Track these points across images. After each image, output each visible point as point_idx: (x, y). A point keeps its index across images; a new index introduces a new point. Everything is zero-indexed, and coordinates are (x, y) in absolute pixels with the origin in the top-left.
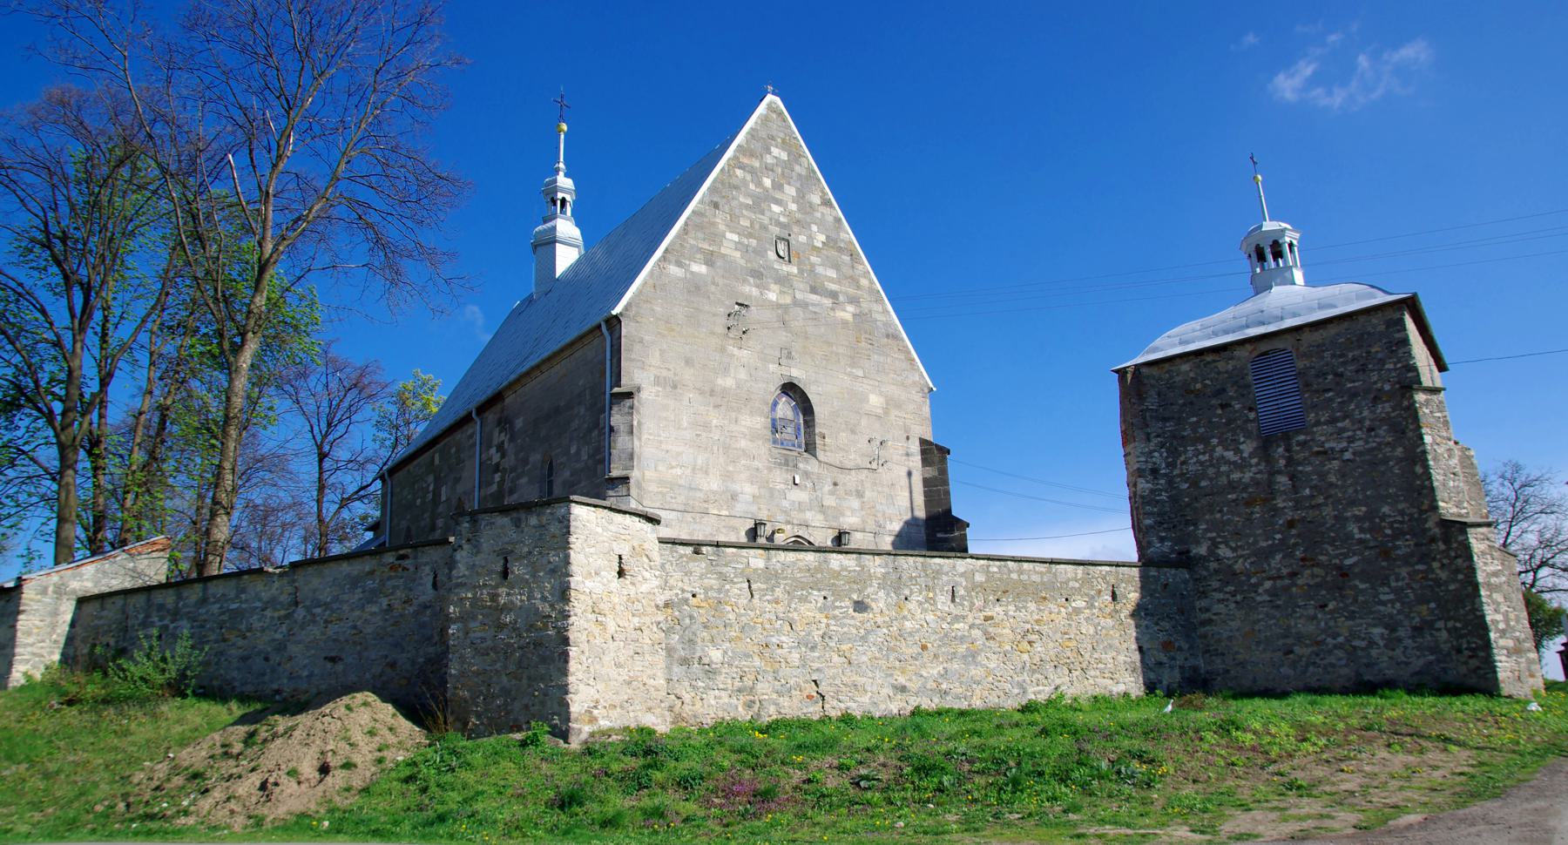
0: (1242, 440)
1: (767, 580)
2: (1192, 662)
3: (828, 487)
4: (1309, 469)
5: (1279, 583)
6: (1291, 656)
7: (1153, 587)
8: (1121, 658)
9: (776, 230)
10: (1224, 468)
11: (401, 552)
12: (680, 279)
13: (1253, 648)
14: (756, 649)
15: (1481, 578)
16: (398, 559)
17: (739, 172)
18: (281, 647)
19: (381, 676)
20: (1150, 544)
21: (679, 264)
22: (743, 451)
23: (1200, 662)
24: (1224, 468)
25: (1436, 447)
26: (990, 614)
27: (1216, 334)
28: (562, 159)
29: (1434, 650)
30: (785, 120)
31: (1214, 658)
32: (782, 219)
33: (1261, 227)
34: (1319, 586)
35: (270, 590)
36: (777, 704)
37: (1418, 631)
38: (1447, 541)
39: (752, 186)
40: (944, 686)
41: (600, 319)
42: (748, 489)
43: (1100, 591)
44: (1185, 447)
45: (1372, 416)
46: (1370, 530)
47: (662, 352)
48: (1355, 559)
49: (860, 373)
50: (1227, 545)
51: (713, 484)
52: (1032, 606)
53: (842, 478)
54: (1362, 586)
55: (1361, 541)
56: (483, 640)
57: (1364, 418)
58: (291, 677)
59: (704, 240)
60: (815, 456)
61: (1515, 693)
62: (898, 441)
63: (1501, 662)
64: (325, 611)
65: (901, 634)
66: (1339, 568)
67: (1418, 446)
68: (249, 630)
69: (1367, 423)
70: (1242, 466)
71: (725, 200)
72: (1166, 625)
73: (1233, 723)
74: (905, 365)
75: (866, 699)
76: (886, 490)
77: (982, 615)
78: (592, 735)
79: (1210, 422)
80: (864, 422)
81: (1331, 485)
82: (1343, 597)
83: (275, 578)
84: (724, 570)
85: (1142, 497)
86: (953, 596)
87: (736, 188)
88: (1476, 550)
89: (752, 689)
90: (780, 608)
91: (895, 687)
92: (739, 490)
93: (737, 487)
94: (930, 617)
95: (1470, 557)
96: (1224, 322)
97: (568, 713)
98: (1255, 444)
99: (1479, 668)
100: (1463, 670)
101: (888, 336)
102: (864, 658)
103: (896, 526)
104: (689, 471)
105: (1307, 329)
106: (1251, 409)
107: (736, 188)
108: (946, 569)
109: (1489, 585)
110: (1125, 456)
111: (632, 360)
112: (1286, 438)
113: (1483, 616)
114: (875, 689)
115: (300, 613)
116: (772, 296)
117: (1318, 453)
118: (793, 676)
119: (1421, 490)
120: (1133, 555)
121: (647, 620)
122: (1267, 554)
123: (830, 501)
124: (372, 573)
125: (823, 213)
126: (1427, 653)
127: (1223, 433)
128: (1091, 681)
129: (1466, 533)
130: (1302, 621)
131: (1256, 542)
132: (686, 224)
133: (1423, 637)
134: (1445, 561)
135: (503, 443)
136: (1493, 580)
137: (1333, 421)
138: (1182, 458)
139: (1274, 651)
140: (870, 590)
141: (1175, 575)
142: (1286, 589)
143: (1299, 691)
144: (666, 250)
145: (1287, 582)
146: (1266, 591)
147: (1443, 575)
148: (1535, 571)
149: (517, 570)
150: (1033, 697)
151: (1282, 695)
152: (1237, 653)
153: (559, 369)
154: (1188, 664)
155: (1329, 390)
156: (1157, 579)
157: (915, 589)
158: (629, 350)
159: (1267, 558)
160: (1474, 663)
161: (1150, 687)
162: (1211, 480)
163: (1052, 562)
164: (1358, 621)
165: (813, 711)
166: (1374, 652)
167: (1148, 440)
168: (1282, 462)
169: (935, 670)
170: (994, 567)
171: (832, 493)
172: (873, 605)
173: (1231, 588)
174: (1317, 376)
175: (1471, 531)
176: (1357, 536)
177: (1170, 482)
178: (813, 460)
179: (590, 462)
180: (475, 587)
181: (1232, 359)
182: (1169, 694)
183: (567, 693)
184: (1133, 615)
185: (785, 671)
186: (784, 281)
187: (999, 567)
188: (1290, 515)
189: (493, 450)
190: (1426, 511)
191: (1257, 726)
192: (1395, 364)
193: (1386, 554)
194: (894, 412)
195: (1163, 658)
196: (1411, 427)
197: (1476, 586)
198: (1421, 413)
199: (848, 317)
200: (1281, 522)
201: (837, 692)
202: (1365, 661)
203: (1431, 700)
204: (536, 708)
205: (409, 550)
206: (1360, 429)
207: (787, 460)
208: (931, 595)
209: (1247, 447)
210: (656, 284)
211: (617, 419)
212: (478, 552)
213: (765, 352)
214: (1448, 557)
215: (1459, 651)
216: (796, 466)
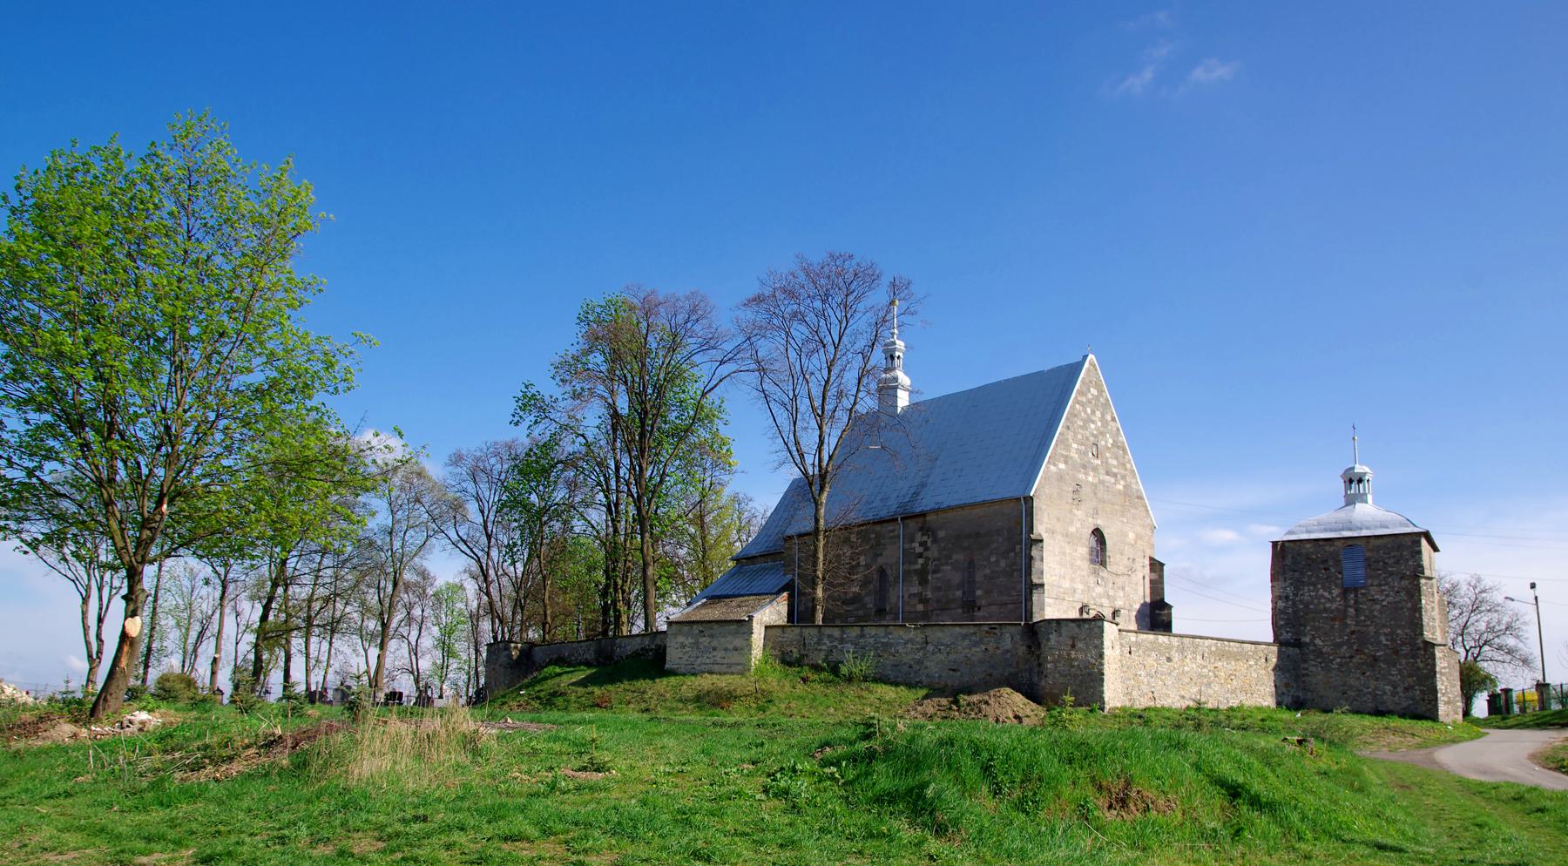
3: (1111, 585)
10: (1323, 601)
15: (1438, 669)
17: (1077, 406)
18: (919, 662)
20: (1281, 634)
21: (1054, 465)
23: (1301, 694)
27: (1326, 530)
34: (1363, 664)
37: (1407, 689)
38: (1425, 651)
42: (1080, 587)
51: (1066, 584)
52: (1233, 663)
55: (1385, 645)
65: (1183, 673)
66: (1374, 656)
70: (1331, 601)
74: (1144, 514)
81: (1375, 616)
87: (1076, 416)
93: (1075, 586)
95: (1434, 659)
103: (1137, 606)
107: (1076, 416)
109: (1441, 673)
112: (1356, 590)
115: (930, 648)
116: (1090, 479)
118: (1145, 689)
119: (1417, 624)
120: (1270, 639)
122: (1340, 645)
124: (975, 633)
137: (1380, 585)
142: (1347, 663)
147: (1421, 665)
148: (1481, 647)
149: (1080, 645)
153: (976, 511)
160: (1429, 706)
161: (1279, 704)
163: (1243, 642)
165: (1152, 704)
166: (1385, 697)
167: (1285, 581)
168: (1352, 602)
170: (1219, 643)
171: (1112, 588)
173: (1319, 660)
177: (1294, 603)
184: (1274, 670)
185: (1143, 687)
186: (1095, 469)
188: (1353, 628)
189: (916, 545)
193: (1396, 652)
194: (1139, 542)
197: (1435, 673)
203: (1408, 721)
209: (1336, 592)
210: (1045, 478)
211: (1034, 553)
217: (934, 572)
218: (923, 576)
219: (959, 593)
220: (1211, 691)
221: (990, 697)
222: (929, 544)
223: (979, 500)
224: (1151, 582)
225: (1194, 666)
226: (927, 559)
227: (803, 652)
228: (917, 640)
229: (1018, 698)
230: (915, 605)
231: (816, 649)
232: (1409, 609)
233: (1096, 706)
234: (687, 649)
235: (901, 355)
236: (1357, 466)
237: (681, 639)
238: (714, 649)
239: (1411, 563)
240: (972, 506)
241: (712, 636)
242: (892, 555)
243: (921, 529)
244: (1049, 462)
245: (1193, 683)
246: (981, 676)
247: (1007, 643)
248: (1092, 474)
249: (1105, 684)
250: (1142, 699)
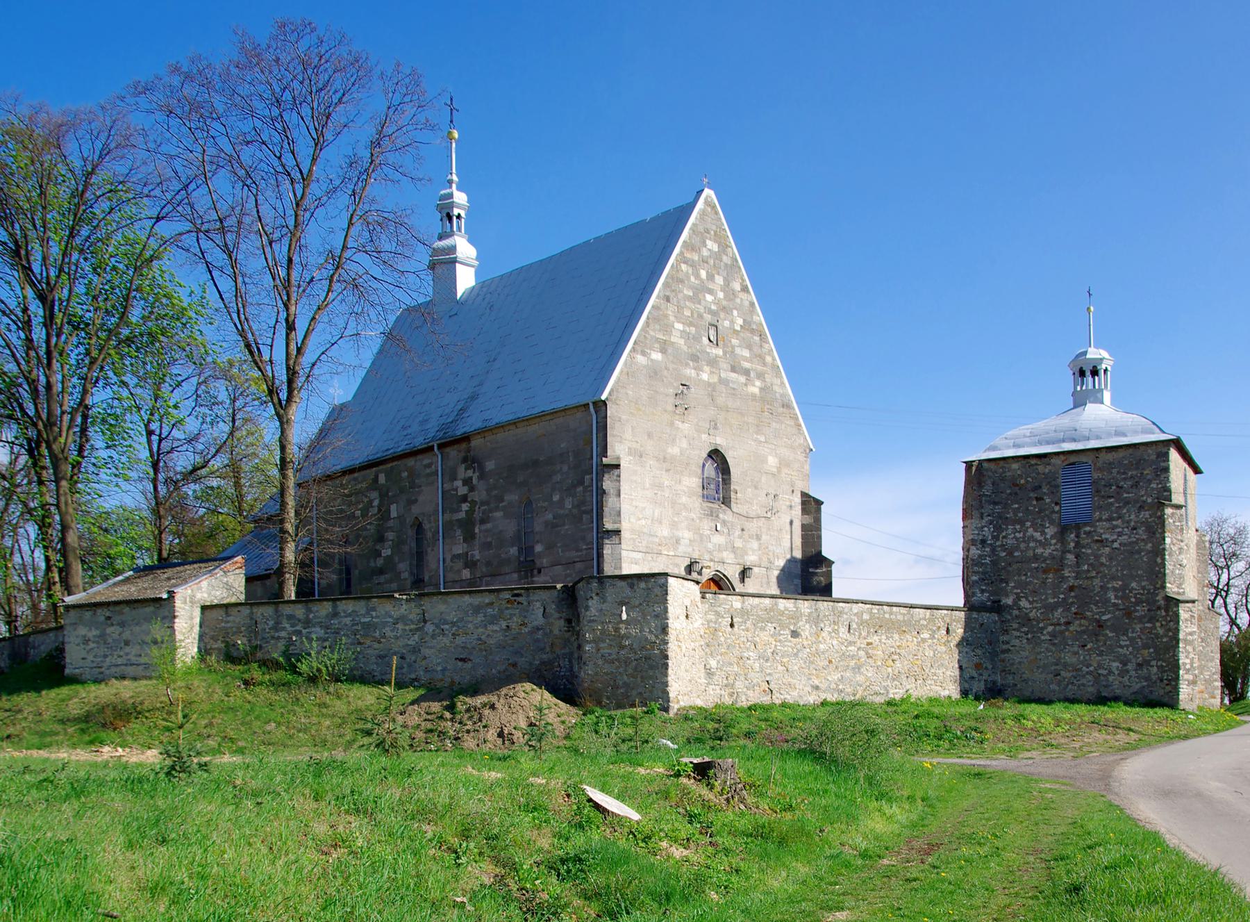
0: (1047, 525)
1: (742, 616)
2: (993, 677)
3: (738, 533)
4: (1089, 551)
5: (1058, 628)
6: (1058, 677)
7: (973, 625)
8: (948, 673)
9: (708, 317)
10: (1032, 544)
11: (515, 592)
12: (645, 367)
13: (1035, 670)
14: (735, 660)
15: (1181, 636)
16: (512, 596)
17: (684, 267)
18: (415, 650)
19: (504, 671)
20: (974, 594)
21: (644, 354)
22: (684, 505)
23: (998, 678)
24: (1032, 544)
25: (1172, 546)
26: (870, 641)
27: (1040, 443)
28: (454, 171)
29: (1147, 679)
30: (717, 213)
31: (1007, 675)
32: (713, 307)
33: (1085, 353)
34: (1084, 632)
35: (399, 609)
36: (746, 695)
37: (1140, 665)
38: (1167, 611)
39: (692, 279)
40: (840, 687)
41: (589, 399)
42: (686, 535)
43: (939, 627)
44: (1007, 525)
45: (1136, 519)
46: (1121, 598)
47: (633, 428)
48: (1109, 616)
49: (763, 439)
50: (1027, 599)
51: (664, 531)
52: (896, 636)
53: (748, 525)
54: (1110, 635)
55: (1115, 605)
56: (610, 654)
57: (1131, 520)
58: (426, 670)
59: (660, 331)
60: (730, 508)
62: (786, 494)
64: (453, 627)
65: (817, 653)
66: (1098, 621)
67: (1161, 545)
68: (384, 637)
69: (1132, 524)
71: (674, 294)
72: (979, 652)
73: (1022, 716)
75: (795, 693)
76: (776, 533)
77: (865, 641)
78: (678, 710)
79: (1027, 509)
80: (764, 479)
81: (1102, 564)
82: (1097, 640)
83: (403, 602)
84: (719, 609)
85: (973, 560)
86: (849, 629)
87: (682, 281)
89: (733, 685)
90: (749, 634)
91: (812, 686)
92: (681, 535)
93: (680, 534)
94: (835, 642)
95: (1178, 623)
96: (1047, 433)
97: (669, 698)
98: (1056, 530)
99: (1170, 692)
100: (1162, 692)
101: (783, 406)
102: (796, 668)
103: (781, 563)
104: (650, 521)
105: (1104, 450)
106: (1057, 504)
108: (846, 610)
110: (963, 527)
111: (614, 436)
112: (1078, 527)
113: (1178, 660)
114: (801, 687)
115: (429, 628)
116: (705, 377)
117: (1097, 541)
118: (756, 677)
119: (1157, 574)
120: (960, 602)
121: (697, 644)
123: (738, 543)
124: (492, 604)
125: (741, 299)
127: (1035, 519)
128: (928, 687)
129: (1178, 606)
130: (1069, 655)
131: (1046, 599)
132: (648, 318)
134: (1163, 623)
135: (471, 478)
136: (1189, 638)
137: (1110, 519)
138: (1004, 534)
139: (1048, 673)
140: (801, 623)
141: (989, 617)
142: (1062, 632)
143: (1059, 701)
144: (635, 343)
145: (1063, 627)
146: (1048, 633)
147: (1161, 631)
150: (892, 696)
151: (1049, 702)
152: (1024, 673)
153: (535, 429)
154: (990, 679)
156: (977, 619)
157: (827, 623)
158: (612, 428)
159: (1052, 610)
160: (1168, 688)
161: (965, 693)
162: (1022, 551)
163: (912, 607)
164: (1104, 657)
165: (766, 700)
166: (1111, 678)
168: (1072, 544)
169: (836, 676)
170: (875, 609)
171: (740, 537)
172: (802, 633)
174: (1105, 486)
176: (1113, 601)
177: (993, 550)
178: (729, 511)
179: (575, 511)
180: (603, 623)
181: (1049, 464)
182: (977, 698)
183: (667, 686)
184: (958, 645)
185: (751, 675)
186: (713, 362)
187: (878, 610)
188: (1072, 582)
189: (459, 483)
190: (1158, 589)
191: (1035, 718)
192: (1158, 484)
193: (1128, 614)
194: (784, 471)
196: (1160, 531)
197: (1178, 641)
198: (1167, 522)
199: (756, 390)
200: (1065, 587)
201: (780, 689)
202: (1104, 683)
204: (647, 694)
205: (523, 591)
206: (1127, 528)
207: (712, 512)
208: (836, 628)
209: (1050, 531)
210: (627, 373)
211: (607, 484)
212: (604, 602)
213: (700, 424)
214: (1166, 620)
215: (1162, 680)
216: (717, 516)
217: (483, 522)
218: (467, 526)
219: (514, 551)
220: (860, 678)
221: (499, 696)
222: (475, 481)
223: (535, 411)
224: (804, 527)
225: (835, 642)
226: (473, 503)
227: (255, 643)
228: (411, 617)
229: (541, 696)
230: (459, 571)
231: (273, 638)
232: (1149, 552)
233: (655, 706)
234: (92, 645)
235: (463, 214)
236: (1090, 350)
237: (82, 631)
238: (127, 643)
239: (1154, 486)
240: (527, 420)
241: (122, 624)
242: (430, 499)
243: (465, 460)
244: (634, 350)
245: (832, 667)
246: (501, 668)
247: (537, 618)
248: (707, 368)
249: (670, 671)
250: (750, 693)
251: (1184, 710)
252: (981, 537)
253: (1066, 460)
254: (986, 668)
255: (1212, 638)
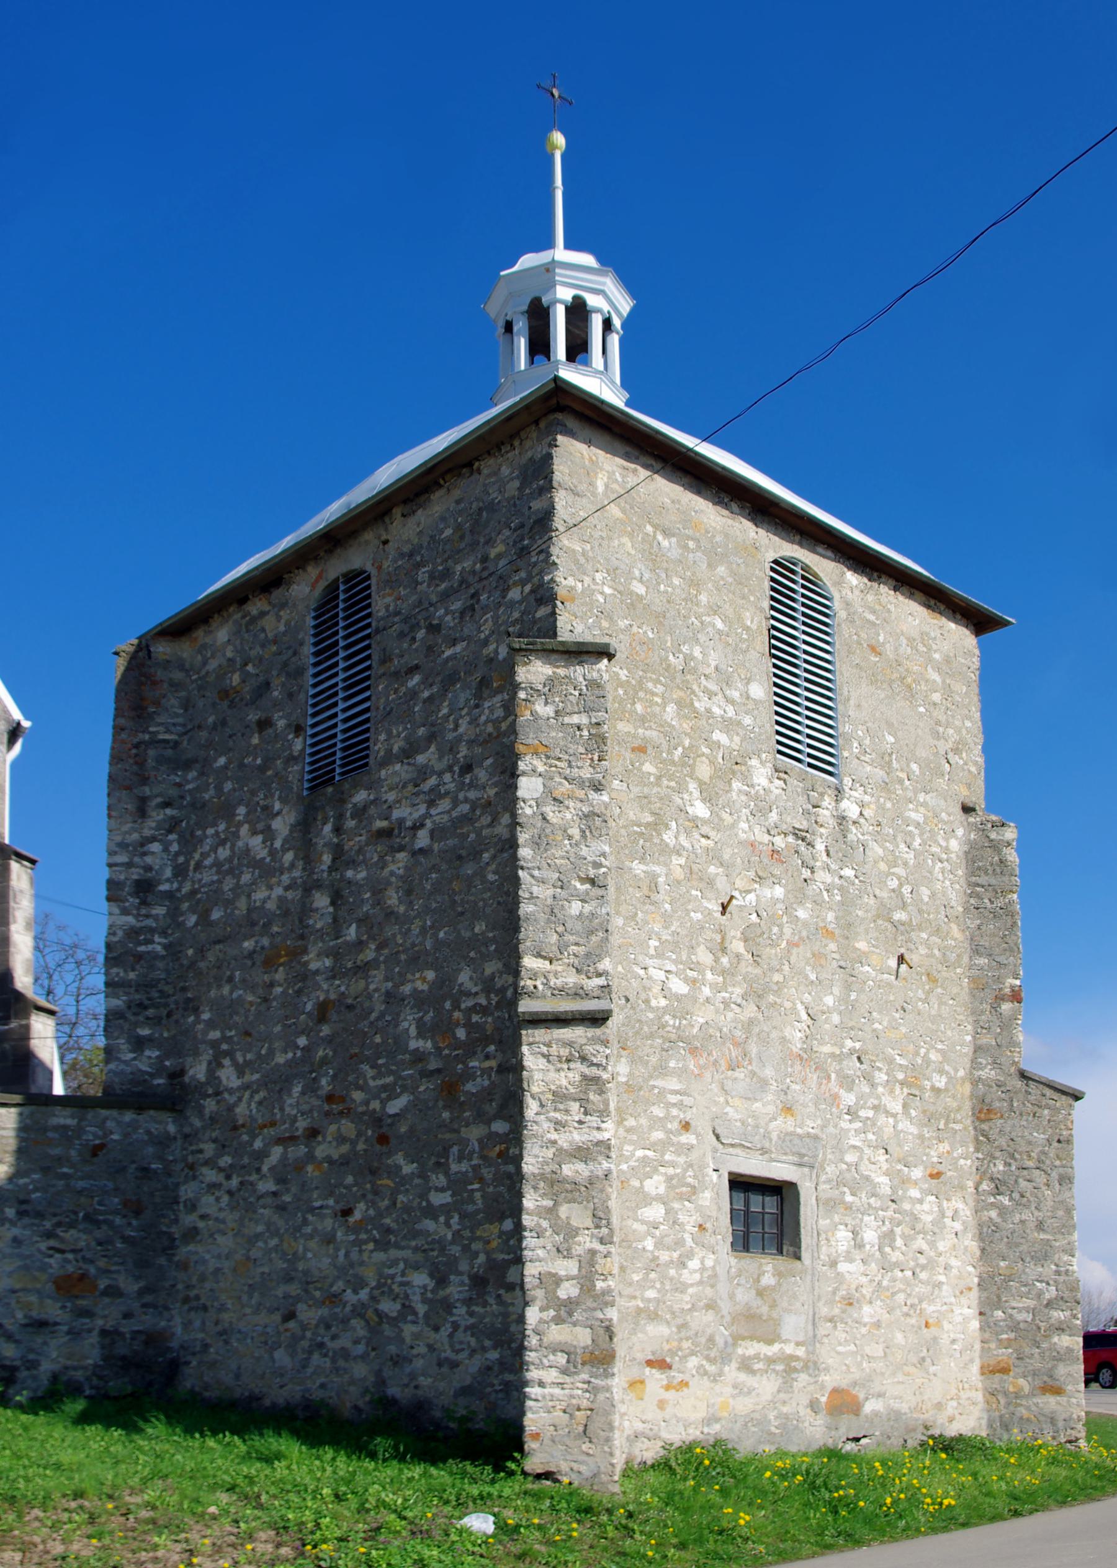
7: (56, 1151)
15: (529, 1166)
25: (549, 810)
55: (419, 1057)
61: (564, 1466)
63: (541, 1384)
66: (377, 1120)
81: (390, 914)
88: (535, 1089)
109: (554, 1183)
126: (487, 1343)
133: (485, 1304)
154: (127, 1327)
155: (413, 670)
164: (394, 1253)
166: (408, 1330)
167: (142, 812)
175: (527, 1035)
176: (413, 1044)
195: (53, 1310)
197: (514, 1181)
198: (525, 716)
251: (548, 1475)
252: (135, 874)
253: (320, 577)
254: (113, 1292)
255: (1040, 1178)
